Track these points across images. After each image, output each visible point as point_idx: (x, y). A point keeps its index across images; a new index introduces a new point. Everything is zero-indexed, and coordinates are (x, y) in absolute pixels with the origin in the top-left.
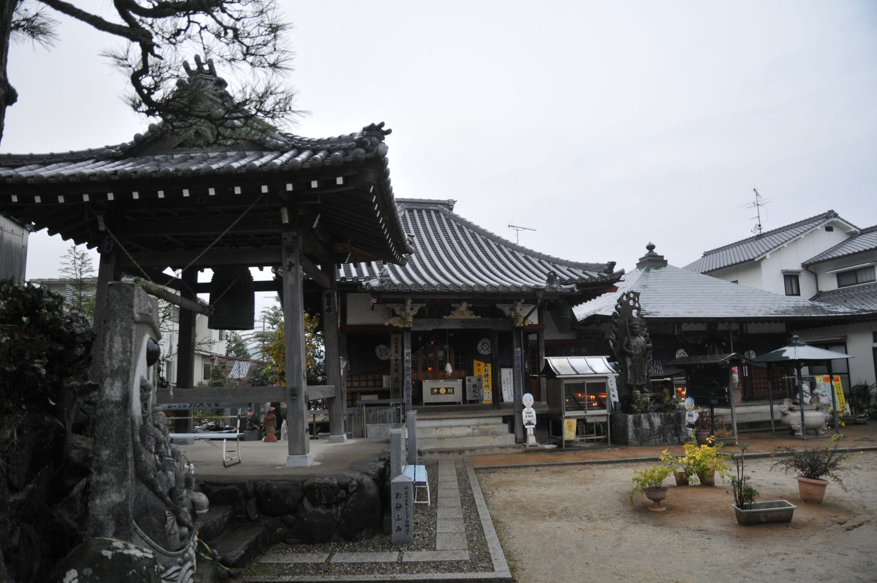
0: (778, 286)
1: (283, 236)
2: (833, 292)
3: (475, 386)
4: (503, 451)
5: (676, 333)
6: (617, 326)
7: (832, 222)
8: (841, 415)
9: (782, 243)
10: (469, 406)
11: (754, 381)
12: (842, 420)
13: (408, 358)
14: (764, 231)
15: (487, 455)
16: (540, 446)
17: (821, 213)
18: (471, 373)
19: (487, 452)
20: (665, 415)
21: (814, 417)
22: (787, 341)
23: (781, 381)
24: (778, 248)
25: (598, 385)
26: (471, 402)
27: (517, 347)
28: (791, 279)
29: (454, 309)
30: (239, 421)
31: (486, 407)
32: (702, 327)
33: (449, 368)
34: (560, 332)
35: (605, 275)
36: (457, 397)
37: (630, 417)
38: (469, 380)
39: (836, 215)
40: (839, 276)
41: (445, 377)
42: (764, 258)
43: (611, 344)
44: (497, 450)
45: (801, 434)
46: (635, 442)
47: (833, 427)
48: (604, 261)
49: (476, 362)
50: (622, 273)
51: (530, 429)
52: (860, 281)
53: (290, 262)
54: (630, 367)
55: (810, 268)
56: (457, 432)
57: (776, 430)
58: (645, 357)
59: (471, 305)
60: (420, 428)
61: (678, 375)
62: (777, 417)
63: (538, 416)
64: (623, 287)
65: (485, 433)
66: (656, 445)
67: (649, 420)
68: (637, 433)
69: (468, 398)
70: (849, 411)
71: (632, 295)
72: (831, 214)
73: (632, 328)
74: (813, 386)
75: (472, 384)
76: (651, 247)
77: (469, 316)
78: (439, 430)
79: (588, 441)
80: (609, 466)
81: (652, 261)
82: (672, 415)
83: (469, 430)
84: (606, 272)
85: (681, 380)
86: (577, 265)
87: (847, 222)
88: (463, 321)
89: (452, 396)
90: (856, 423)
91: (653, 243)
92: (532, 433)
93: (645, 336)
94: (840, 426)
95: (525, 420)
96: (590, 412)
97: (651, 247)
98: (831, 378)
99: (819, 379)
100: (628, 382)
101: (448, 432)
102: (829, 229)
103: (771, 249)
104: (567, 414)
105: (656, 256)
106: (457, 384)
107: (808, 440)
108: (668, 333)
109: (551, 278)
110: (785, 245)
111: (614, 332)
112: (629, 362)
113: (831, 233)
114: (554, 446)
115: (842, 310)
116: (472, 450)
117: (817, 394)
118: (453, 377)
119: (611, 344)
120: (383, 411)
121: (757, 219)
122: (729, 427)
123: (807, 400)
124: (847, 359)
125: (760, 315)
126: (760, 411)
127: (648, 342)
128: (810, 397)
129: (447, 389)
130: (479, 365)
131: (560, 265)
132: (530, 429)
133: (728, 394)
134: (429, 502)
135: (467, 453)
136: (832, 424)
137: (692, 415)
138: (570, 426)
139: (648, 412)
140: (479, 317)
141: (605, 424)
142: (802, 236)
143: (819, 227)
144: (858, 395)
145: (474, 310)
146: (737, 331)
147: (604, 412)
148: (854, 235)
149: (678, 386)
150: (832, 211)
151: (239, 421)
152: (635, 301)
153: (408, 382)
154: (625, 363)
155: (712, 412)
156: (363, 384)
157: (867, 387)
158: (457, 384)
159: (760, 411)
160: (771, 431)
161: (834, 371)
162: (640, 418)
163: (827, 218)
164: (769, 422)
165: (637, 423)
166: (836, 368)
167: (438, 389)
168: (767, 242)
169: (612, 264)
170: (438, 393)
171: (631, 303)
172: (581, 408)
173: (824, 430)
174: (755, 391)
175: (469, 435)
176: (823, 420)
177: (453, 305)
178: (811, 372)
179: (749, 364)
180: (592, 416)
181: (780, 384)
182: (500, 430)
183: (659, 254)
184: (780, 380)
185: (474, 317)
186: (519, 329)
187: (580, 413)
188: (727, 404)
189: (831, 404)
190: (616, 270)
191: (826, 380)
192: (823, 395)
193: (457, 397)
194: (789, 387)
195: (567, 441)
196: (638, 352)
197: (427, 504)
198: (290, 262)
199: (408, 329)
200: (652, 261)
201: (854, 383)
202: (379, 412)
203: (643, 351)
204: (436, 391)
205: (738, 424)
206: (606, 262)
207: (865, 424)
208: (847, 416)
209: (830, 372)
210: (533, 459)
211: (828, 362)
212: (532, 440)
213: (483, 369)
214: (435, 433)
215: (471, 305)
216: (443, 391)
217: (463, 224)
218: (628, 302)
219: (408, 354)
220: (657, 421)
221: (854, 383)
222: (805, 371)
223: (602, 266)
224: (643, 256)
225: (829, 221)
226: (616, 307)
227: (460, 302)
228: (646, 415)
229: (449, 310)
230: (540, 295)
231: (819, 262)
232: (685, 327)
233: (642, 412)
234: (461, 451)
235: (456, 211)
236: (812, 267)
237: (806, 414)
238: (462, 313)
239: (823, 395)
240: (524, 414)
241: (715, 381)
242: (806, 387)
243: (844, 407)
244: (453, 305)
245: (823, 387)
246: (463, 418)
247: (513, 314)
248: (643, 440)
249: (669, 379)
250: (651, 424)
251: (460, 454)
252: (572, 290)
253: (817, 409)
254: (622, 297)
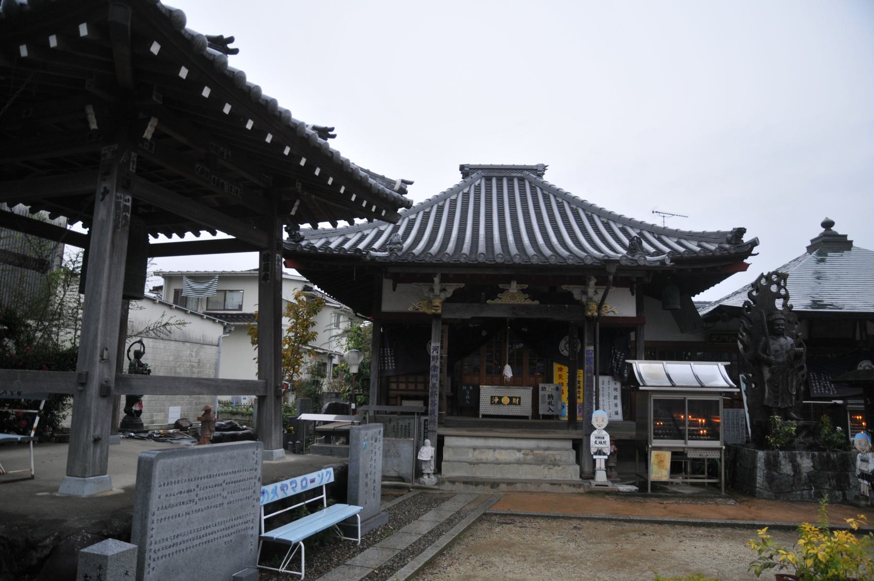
1: (103, 152)
3: (550, 396)
4: (556, 489)
5: (858, 337)
6: (751, 322)
10: (538, 422)
13: (435, 354)
15: (532, 493)
16: (611, 486)
18: (549, 380)
19: (532, 488)
20: (820, 456)
26: (545, 417)
27: (589, 345)
29: (502, 291)
30: (37, 419)
31: (559, 426)
33: (508, 372)
34: (682, 332)
35: (727, 246)
36: (525, 408)
37: (761, 454)
38: (544, 389)
41: (502, 382)
43: (741, 346)
44: (546, 487)
49: (556, 366)
51: (600, 461)
53: (105, 188)
54: (769, 381)
56: (503, 456)
59: (526, 286)
60: (455, 448)
61: (854, 397)
63: (613, 442)
64: (758, 266)
65: (541, 461)
66: (803, 501)
67: (793, 460)
68: (770, 479)
69: (541, 412)
73: (772, 324)
75: (547, 393)
77: (522, 300)
78: (477, 452)
79: (693, 484)
80: (701, 531)
82: (834, 456)
83: (519, 455)
84: (729, 242)
86: (691, 236)
88: (513, 307)
89: (518, 407)
91: (831, 218)
96: (692, 443)
100: (766, 403)
101: (490, 456)
104: (656, 443)
105: (836, 235)
106: (525, 394)
111: (745, 330)
112: (767, 375)
114: (633, 488)
116: (510, 483)
118: (515, 382)
119: (741, 346)
120: (407, 421)
127: (800, 345)
129: (511, 398)
130: (560, 370)
131: (667, 236)
132: (600, 461)
134: (303, 574)
135: (503, 487)
138: (661, 462)
139: (794, 448)
140: (537, 302)
145: (531, 293)
147: (716, 444)
151: (37, 419)
153: (434, 385)
156: (402, 386)
158: (525, 394)
162: (776, 456)
165: (772, 464)
167: (500, 398)
170: (500, 402)
172: (680, 436)
175: (519, 463)
177: (501, 286)
180: (696, 449)
182: (563, 459)
183: (840, 233)
185: (529, 302)
186: (591, 319)
187: (678, 443)
190: (746, 238)
193: (525, 408)
196: (780, 360)
197: (300, 576)
198: (105, 188)
199: (436, 316)
202: (401, 423)
204: (497, 400)
206: (730, 229)
210: (602, 507)
212: (601, 477)
213: (560, 374)
214: (471, 456)
215: (526, 286)
216: (506, 400)
217: (551, 192)
219: (435, 349)
220: (806, 463)
223: (725, 233)
224: (816, 235)
226: (750, 295)
227: (508, 280)
228: (787, 453)
229: (494, 293)
230: (612, 269)
233: (782, 449)
234: (494, 484)
235: (548, 178)
238: (513, 296)
240: (593, 438)
244: (501, 286)
246: (516, 438)
247: (584, 299)
248: (782, 491)
249: (840, 402)
250: (796, 468)
251: (492, 487)
252: (662, 262)
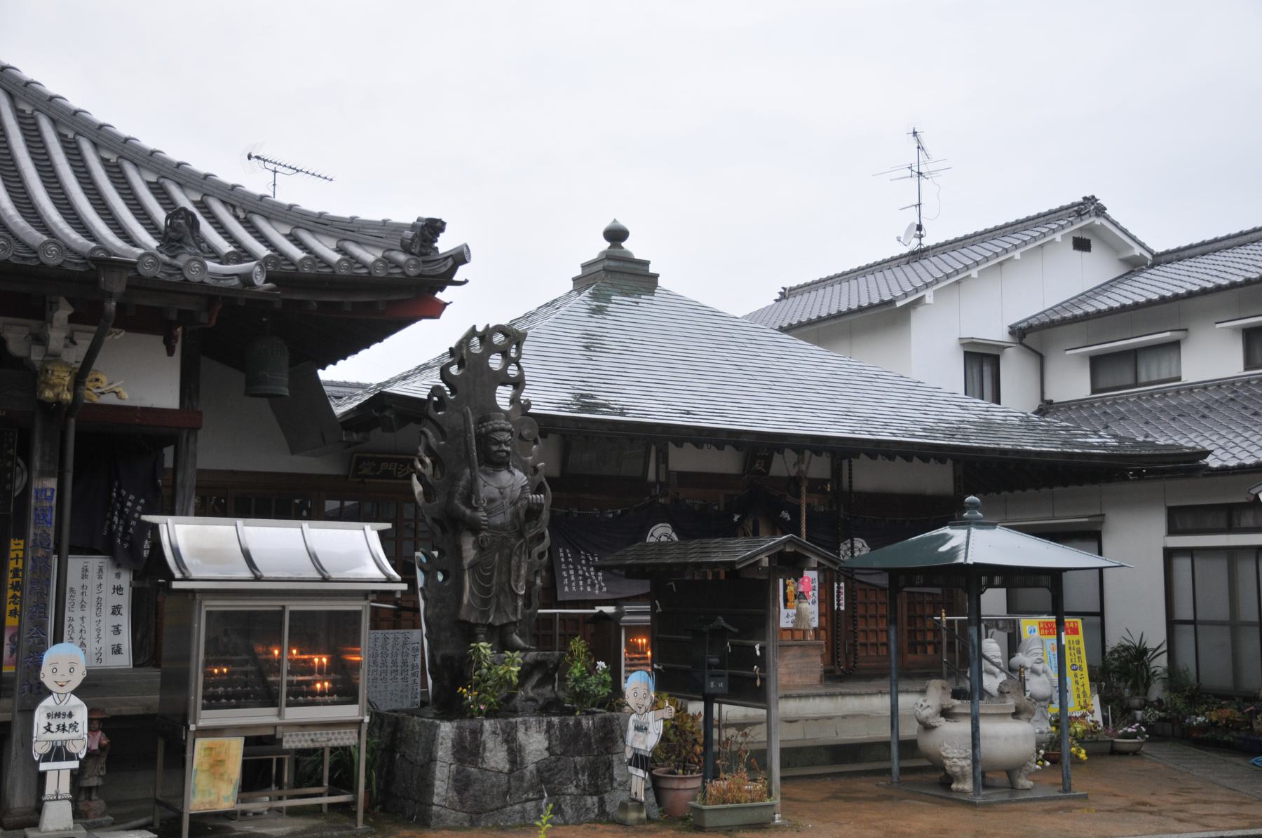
0: (952, 375)
2: (1079, 404)
5: (652, 476)
6: (441, 432)
7: (1089, 228)
8: (1079, 728)
9: (967, 267)
11: (861, 625)
12: (1081, 741)
14: (928, 241)
17: (1067, 203)
20: (563, 725)
21: (1010, 737)
22: (947, 511)
23: (924, 623)
24: (956, 281)
25: (326, 620)
27: (44, 474)
28: (981, 361)
32: (726, 463)
34: (293, 451)
35: (401, 257)
37: (447, 729)
39: (1100, 211)
40: (1097, 363)
42: (919, 302)
43: (418, 488)
45: (968, 786)
46: (452, 816)
47: (1056, 761)
48: (406, 214)
50: (460, 257)
51: (58, 776)
52: (1143, 378)
54: (473, 566)
55: (1030, 339)
57: (904, 771)
58: (521, 534)
62: (909, 730)
64: (466, 309)
68: (461, 784)
70: (1098, 717)
71: (498, 338)
72: (1090, 207)
73: (485, 440)
74: (1014, 644)
76: (616, 235)
79: (294, 812)
81: (618, 274)
82: (587, 723)
84: (406, 249)
85: (637, 614)
87: (1125, 232)
90: (1115, 752)
91: (624, 223)
92: (65, 788)
93: (532, 471)
94: (1075, 760)
95: (42, 741)
97: (616, 235)
98: (1060, 624)
99: (1030, 626)
100: (463, 615)
102: (1081, 244)
103: (937, 281)
104: (208, 718)
105: (630, 260)
107: (987, 806)
108: (613, 476)
109: (178, 234)
110: (974, 273)
111: (429, 451)
112: (469, 552)
113: (1085, 254)
115: (1098, 440)
117: (1020, 669)
119: (418, 488)
121: (914, 211)
122: (758, 761)
123: (991, 683)
124: (1101, 570)
125: (885, 436)
126: (862, 712)
128: (1003, 677)
131: (268, 218)
132: (58, 776)
133: (762, 662)
136: (1052, 751)
137: (645, 727)
138: (217, 764)
139: (515, 712)
141: (343, 758)
142: (1017, 255)
143: (1058, 237)
144: (1119, 672)
146: (824, 481)
147: (350, 712)
148: (1137, 265)
149: (634, 630)
150: (1091, 200)
152: (508, 360)
154: (458, 551)
155: (708, 710)
157: (1145, 651)
159: (862, 712)
160: (888, 771)
161: (1068, 607)
162: (477, 732)
163: (1079, 214)
164: (886, 745)
165: (468, 750)
166: (1077, 595)
168: (932, 268)
169: (433, 228)
171: (495, 362)
173: (1030, 775)
174: (862, 653)
176: (1031, 746)
178: (1012, 607)
179: (848, 574)
180: (303, 726)
181: (930, 637)
183: (638, 256)
184: (929, 624)
188: (750, 689)
189: (1056, 696)
191: (1045, 629)
192: (1034, 672)
194: (951, 645)
195: (197, 819)
196: (498, 520)
200: (618, 274)
201: (1114, 639)
203: (516, 515)
205: (783, 751)
206: (410, 219)
207: (1135, 753)
208: (1092, 731)
209: (1058, 609)
211: (1053, 577)
218: (484, 357)
221: (1114, 639)
222: (993, 601)
223: (399, 228)
225: (1084, 224)
231: (1053, 324)
232: (683, 460)
233: (490, 714)
236: (1034, 337)
237: (986, 727)
239: (1034, 672)
240: (40, 718)
241: (721, 621)
242: (993, 647)
243: (1085, 705)
245: (1036, 648)
249: (609, 610)
250: (515, 754)
252: (246, 279)
253: (1016, 715)
254: (465, 341)
